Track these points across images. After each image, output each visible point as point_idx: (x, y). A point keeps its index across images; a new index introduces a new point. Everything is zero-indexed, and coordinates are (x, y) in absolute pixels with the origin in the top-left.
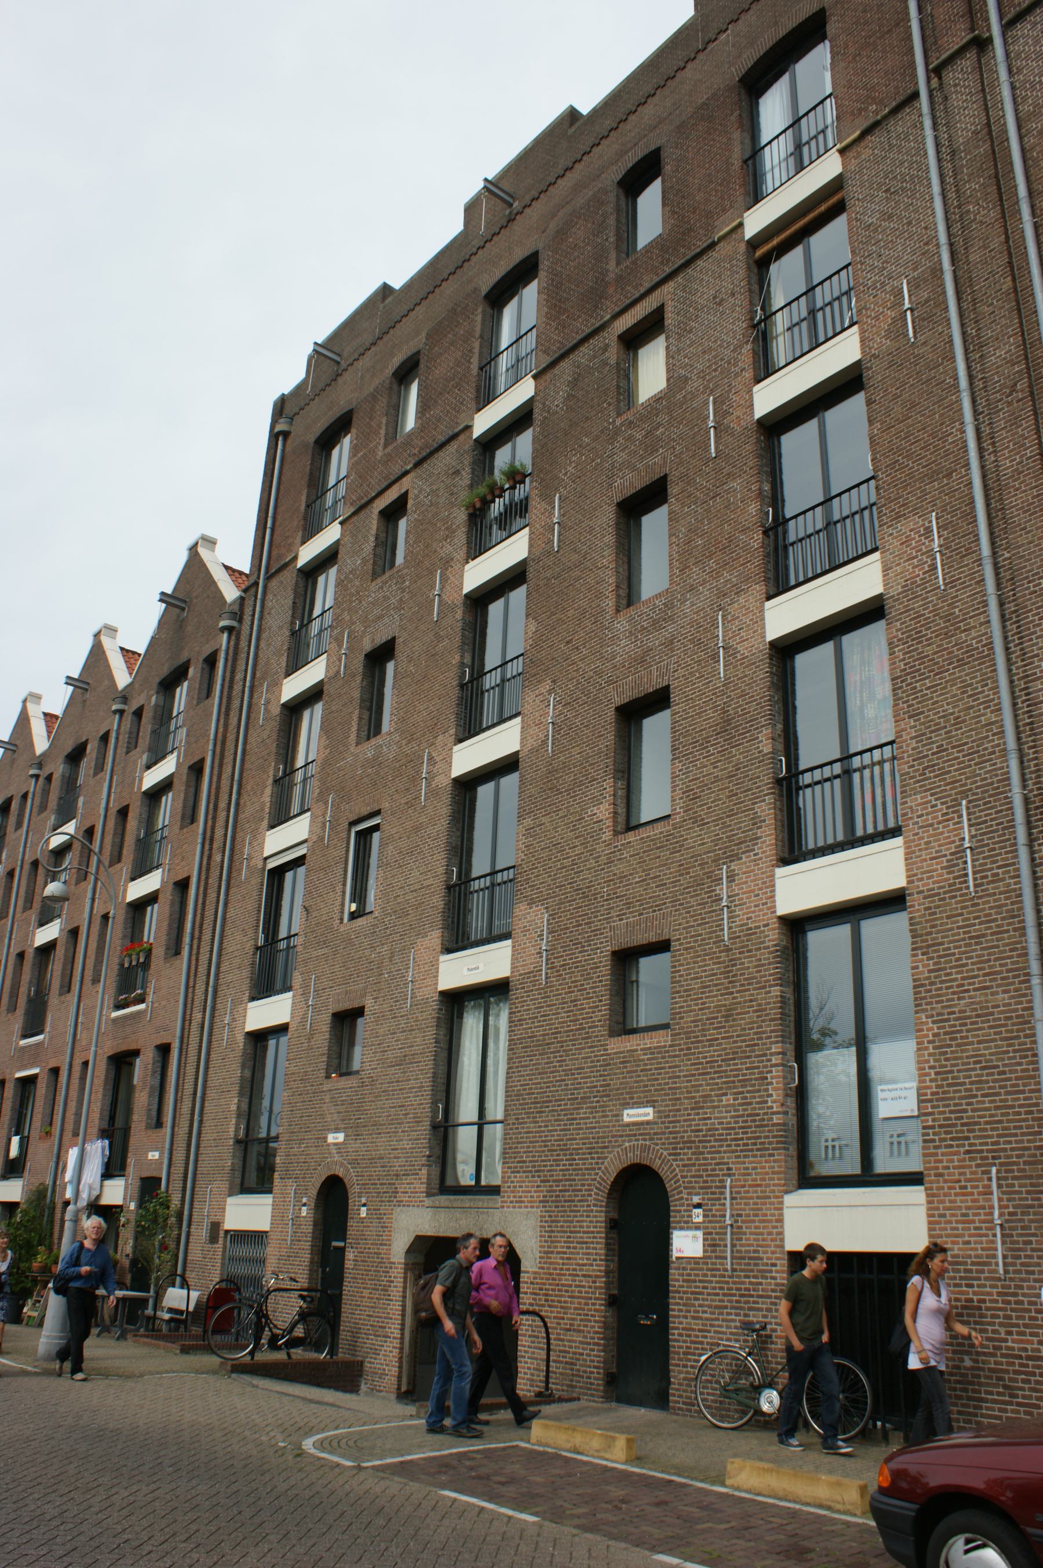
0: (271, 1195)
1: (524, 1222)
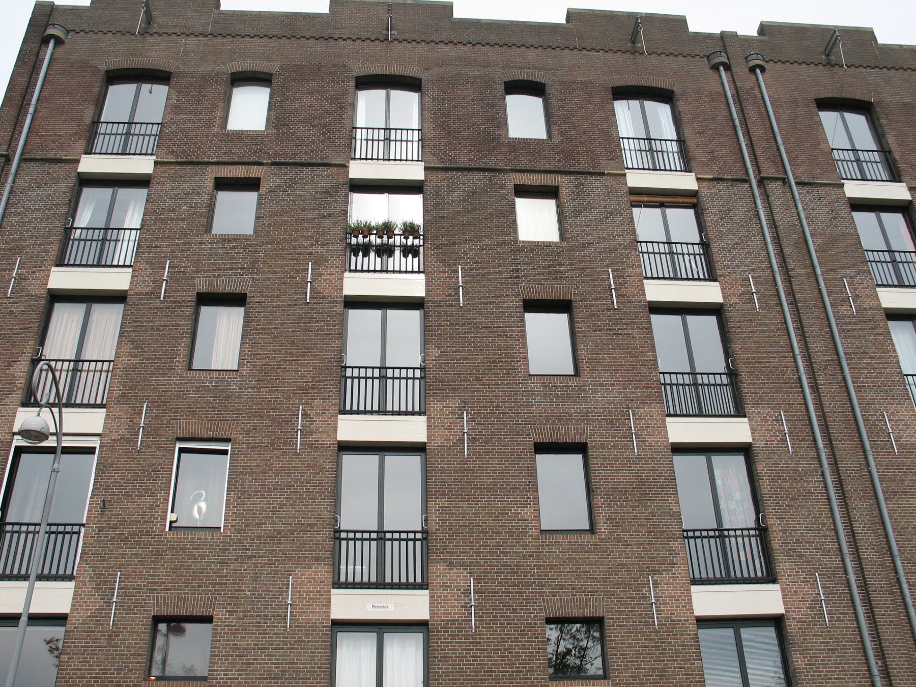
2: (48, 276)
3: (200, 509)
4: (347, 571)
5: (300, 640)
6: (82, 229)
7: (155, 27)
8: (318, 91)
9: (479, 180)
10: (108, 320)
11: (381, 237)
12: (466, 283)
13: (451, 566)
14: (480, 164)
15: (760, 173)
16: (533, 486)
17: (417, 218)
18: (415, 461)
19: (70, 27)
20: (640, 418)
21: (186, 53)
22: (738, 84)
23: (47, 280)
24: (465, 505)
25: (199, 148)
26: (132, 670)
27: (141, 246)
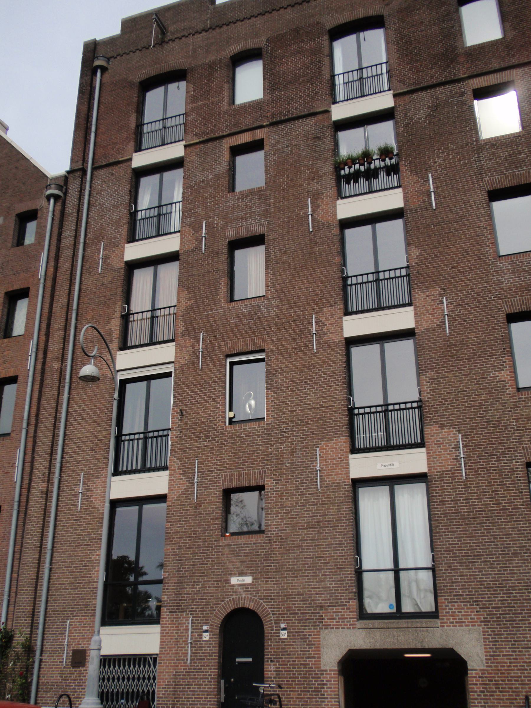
0: (159, 626)
1: (467, 636)
2: (123, 252)
3: (250, 406)
6: (146, 210)
7: (169, 36)
8: (299, 52)
9: (441, 93)
10: (170, 273)
13: (442, 426)
14: (442, 79)
16: (509, 350)
17: (392, 142)
18: (408, 345)
19: (109, 55)
21: (194, 50)
23: (123, 255)
25: (215, 126)
26: (212, 530)
27: (186, 214)
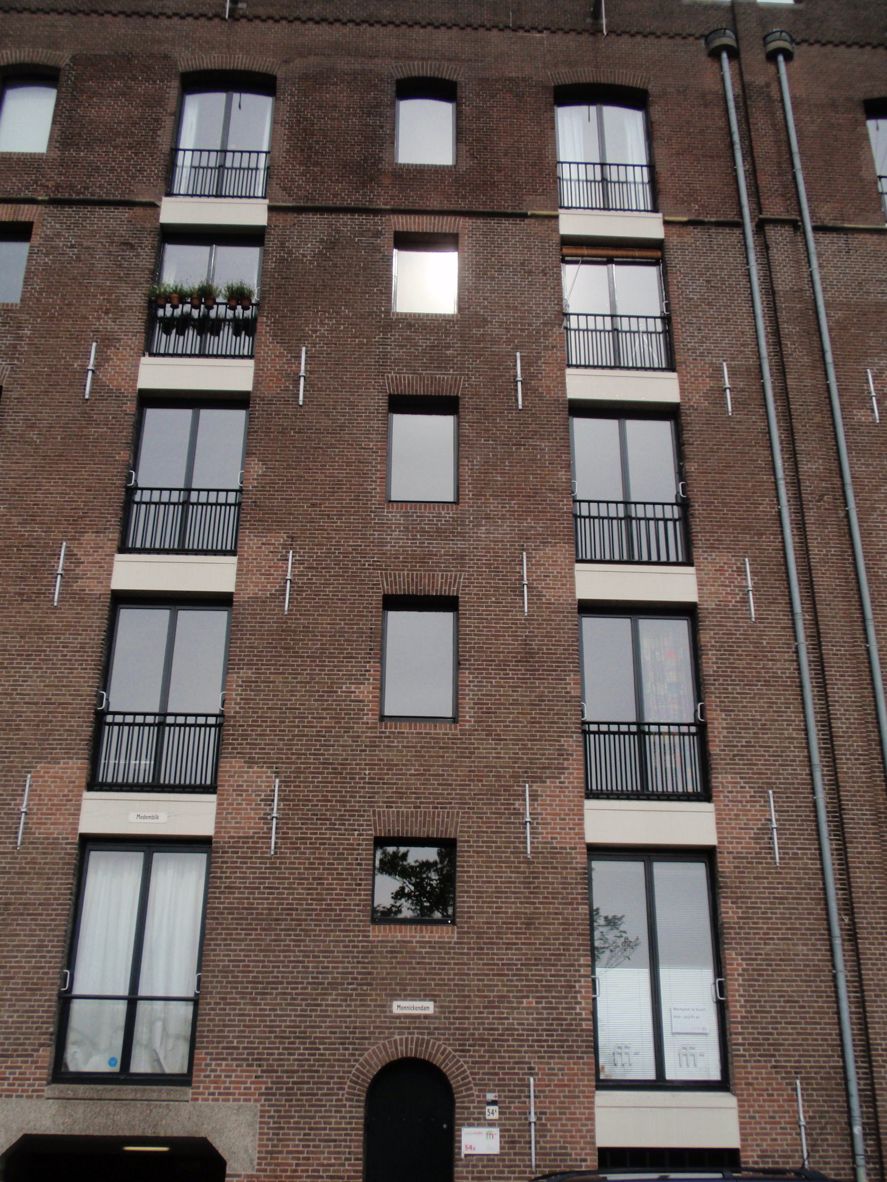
4: (112, 766)
5: (33, 862)
8: (124, 95)
9: (345, 225)
11: (234, 308)
12: (311, 372)
13: (251, 762)
15: (761, 212)
20: (538, 564)
22: (747, 78)
24: (280, 678)
